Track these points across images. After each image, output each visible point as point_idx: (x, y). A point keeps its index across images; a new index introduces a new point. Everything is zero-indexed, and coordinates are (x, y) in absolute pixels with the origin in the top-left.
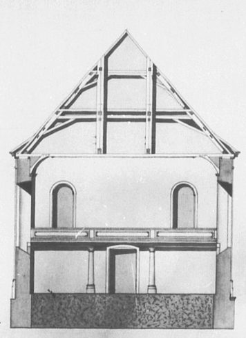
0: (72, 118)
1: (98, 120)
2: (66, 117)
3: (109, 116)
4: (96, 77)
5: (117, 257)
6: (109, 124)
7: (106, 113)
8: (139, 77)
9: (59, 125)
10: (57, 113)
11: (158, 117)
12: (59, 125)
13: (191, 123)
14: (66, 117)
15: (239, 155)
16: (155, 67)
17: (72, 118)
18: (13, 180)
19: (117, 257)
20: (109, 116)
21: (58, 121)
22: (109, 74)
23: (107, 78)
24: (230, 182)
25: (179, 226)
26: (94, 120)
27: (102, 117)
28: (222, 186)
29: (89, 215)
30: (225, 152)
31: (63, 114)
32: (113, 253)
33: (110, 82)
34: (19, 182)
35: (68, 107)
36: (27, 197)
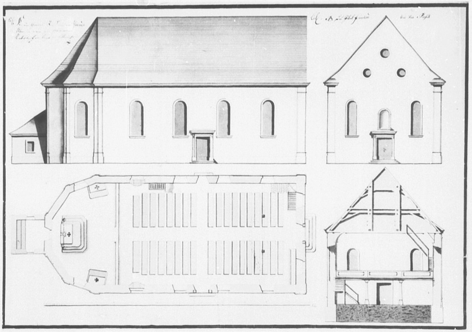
0: (357, 212)
1: (396, 214)
2: (353, 212)
3: (375, 212)
4: (367, 192)
5: (206, 141)
6: (402, 216)
7: (401, 210)
8: (391, 191)
9: (349, 216)
10: (348, 210)
11: (403, 212)
12: (349, 216)
13: (418, 215)
14: (351, 214)
15: (444, 232)
16: (401, 186)
17: (357, 212)
18: (99, 16)
19: (206, 141)
20: (375, 212)
21: (349, 213)
22: (375, 190)
23: (373, 192)
24: (440, 247)
25: (413, 270)
26: (394, 214)
27: (371, 212)
28: (437, 250)
29: (366, 264)
30: (437, 231)
31: (351, 210)
32: (379, 285)
33: (375, 193)
34: (328, 246)
35: (353, 207)
36: (333, 254)
